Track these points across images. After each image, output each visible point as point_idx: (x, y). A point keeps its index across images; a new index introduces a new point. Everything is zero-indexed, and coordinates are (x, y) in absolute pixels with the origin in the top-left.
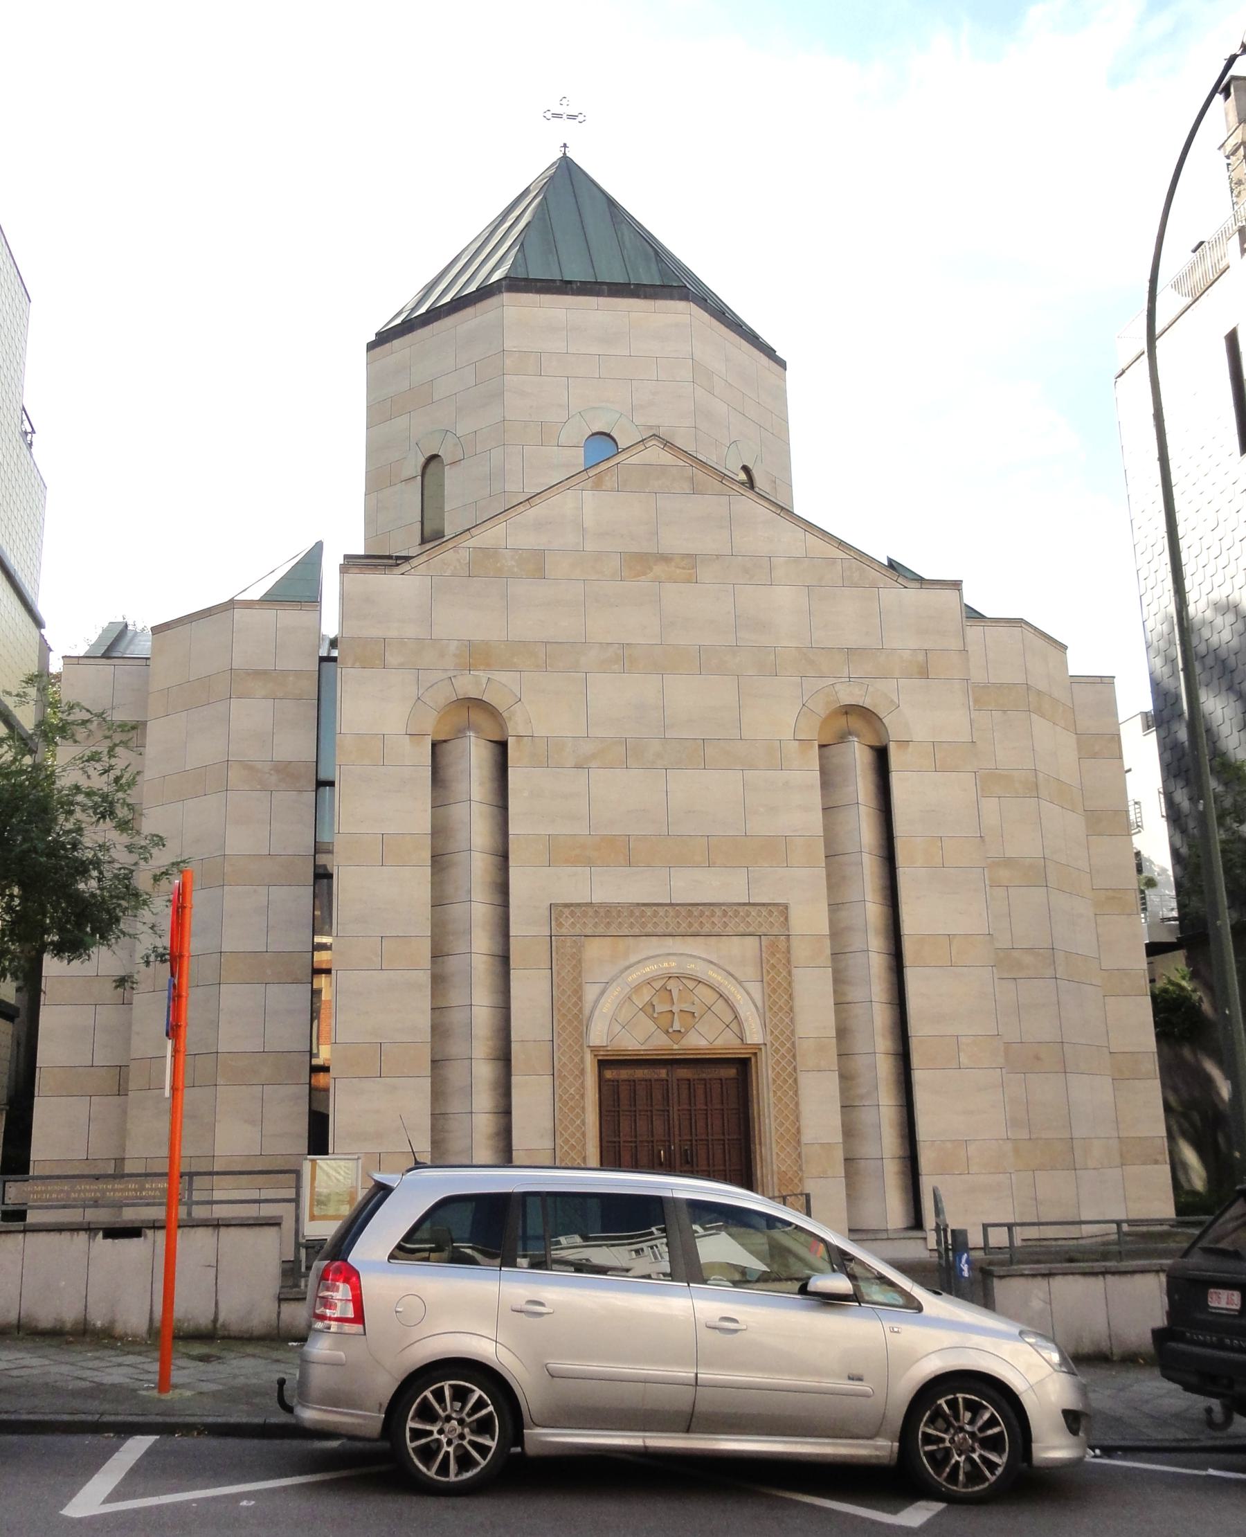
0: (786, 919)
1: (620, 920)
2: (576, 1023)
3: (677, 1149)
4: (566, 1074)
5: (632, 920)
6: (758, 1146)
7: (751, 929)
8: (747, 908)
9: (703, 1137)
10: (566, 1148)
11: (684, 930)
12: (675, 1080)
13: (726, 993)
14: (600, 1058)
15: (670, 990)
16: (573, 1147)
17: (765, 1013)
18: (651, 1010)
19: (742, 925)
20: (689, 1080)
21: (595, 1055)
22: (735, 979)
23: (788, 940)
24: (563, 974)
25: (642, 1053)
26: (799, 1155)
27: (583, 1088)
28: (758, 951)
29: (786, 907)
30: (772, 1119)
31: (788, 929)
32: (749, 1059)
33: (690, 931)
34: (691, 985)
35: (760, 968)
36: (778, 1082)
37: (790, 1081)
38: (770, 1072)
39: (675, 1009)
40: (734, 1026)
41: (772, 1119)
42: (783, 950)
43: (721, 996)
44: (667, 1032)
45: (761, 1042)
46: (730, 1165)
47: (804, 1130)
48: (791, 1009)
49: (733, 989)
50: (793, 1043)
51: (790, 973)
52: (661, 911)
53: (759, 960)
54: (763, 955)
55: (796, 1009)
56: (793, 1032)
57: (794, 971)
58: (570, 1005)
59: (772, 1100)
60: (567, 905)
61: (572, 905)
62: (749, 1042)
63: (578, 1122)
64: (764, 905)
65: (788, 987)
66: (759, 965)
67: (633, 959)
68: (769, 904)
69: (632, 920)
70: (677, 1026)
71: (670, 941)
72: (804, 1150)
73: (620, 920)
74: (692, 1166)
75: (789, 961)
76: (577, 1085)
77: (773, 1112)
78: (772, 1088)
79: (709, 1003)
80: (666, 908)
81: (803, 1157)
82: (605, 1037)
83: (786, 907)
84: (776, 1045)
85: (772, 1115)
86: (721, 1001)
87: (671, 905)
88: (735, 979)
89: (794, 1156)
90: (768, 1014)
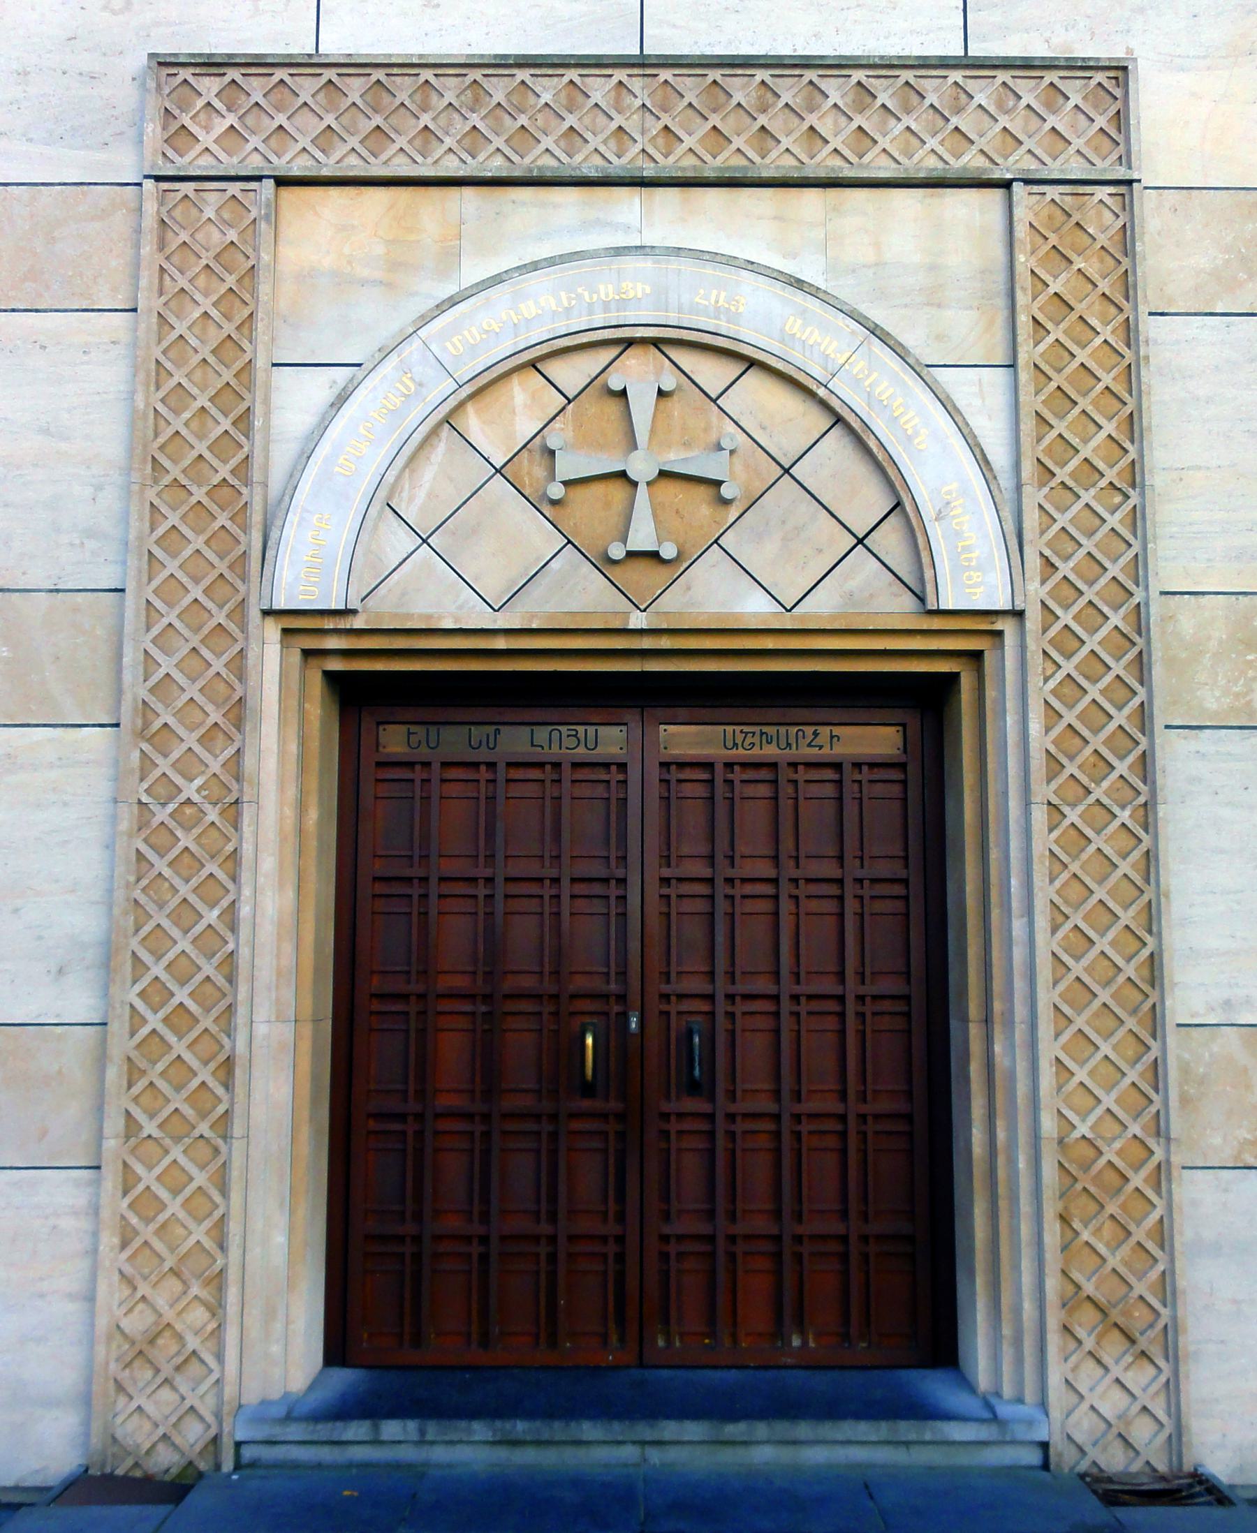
0: (1121, 119)
1: (426, 119)
2: (223, 519)
3: (654, 1026)
4: (171, 721)
5: (475, 119)
6: (975, 1030)
7: (971, 161)
8: (956, 76)
9: (763, 985)
10: (154, 1021)
11: (691, 161)
12: (654, 774)
13: (858, 403)
14: (336, 665)
15: (623, 393)
16: (180, 1019)
17: (1019, 487)
18: (540, 472)
19: (932, 143)
20: (708, 766)
21: (307, 654)
22: (900, 351)
23: (1127, 204)
24: (181, 328)
25: (501, 643)
26: (1156, 1071)
27: (238, 778)
28: (998, 251)
29: (1120, 71)
30: (1042, 922)
31: (1125, 159)
32: (952, 679)
33: (715, 165)
34: (711, 373)
35: (1002, 316)
36: (1071, 768)
37: (1122, 767)
38: (1035, 727)
39: (641, 467)
40: (889, 541)
41: (1042, 922)
42: (1102, 240)
43: (839, 420)
44: (605, 563)
45: (1002, 603)
46: (863, 1097)
47: (1179, 972)
48: (1135, 475)
49: (884, 389)
50: (1139, 616)
51: (1129, 331)
52: (599, 88)
53: (1001, 277)
54: (1021, 258)
55: (1157, 480)
56: (1138, 567)
57: (1151, 328)
58: (202, 448)
59: (1043, 841)
60: (211, 65)
61: (229, 62)
62: (948, 603)
63: (212, 916)
64: (1026, 65)
65: (1119, 389)
66: (1001, 302)
67: (473, 272)
68: (1048, 65)
69: (475, 119)
70: (642, 536)
71: (628, 203)
72: (1176, 1047)
73: (426, 119)
74: (712, 1098)
75: (1128, 285)
76: (215, 766)
77: (1044, 892)
78: (1043, 791)
79: (785, 448)
80: (620, 75)
81: (1173, 1075)
82: (340, 570)
83: (1120, 71)
84: (1066, 618)
85: (1040, 904)
86: (836, 442)
87: (642, 63)
88: (900, 351)
89: (1132, 1076)
90: (1033, 496)
